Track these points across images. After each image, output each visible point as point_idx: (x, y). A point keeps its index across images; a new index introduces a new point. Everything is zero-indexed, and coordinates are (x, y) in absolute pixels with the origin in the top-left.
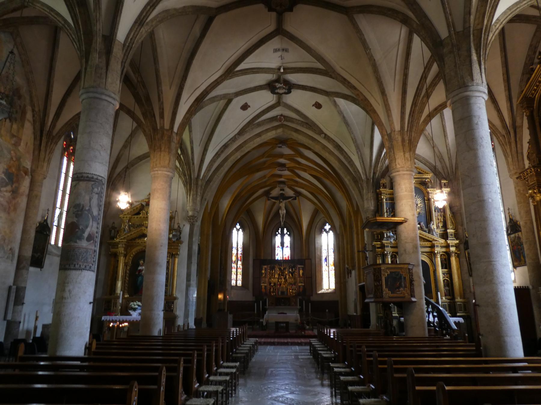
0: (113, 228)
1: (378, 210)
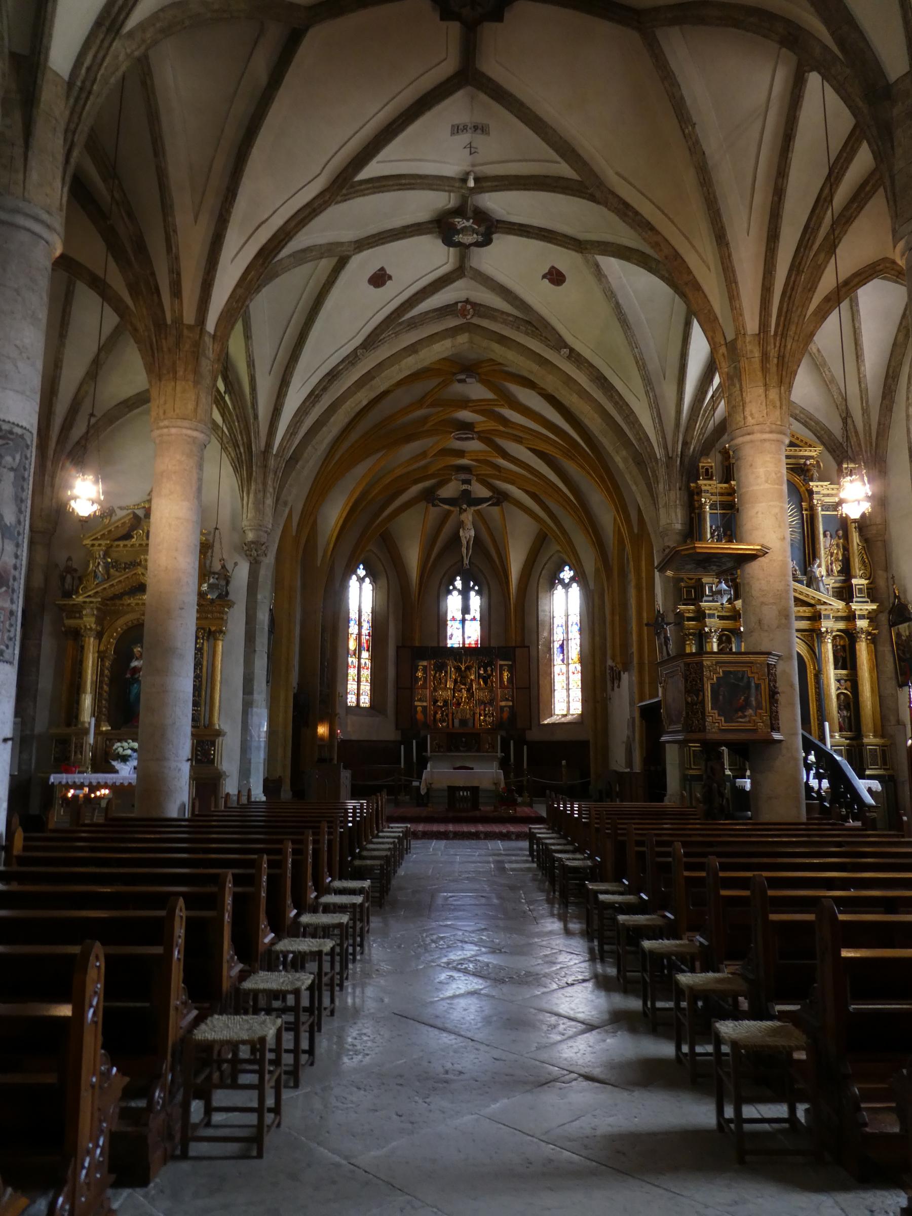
0: (70, 570)
1: (693, 529)
